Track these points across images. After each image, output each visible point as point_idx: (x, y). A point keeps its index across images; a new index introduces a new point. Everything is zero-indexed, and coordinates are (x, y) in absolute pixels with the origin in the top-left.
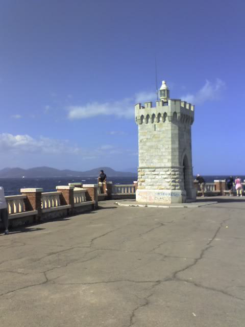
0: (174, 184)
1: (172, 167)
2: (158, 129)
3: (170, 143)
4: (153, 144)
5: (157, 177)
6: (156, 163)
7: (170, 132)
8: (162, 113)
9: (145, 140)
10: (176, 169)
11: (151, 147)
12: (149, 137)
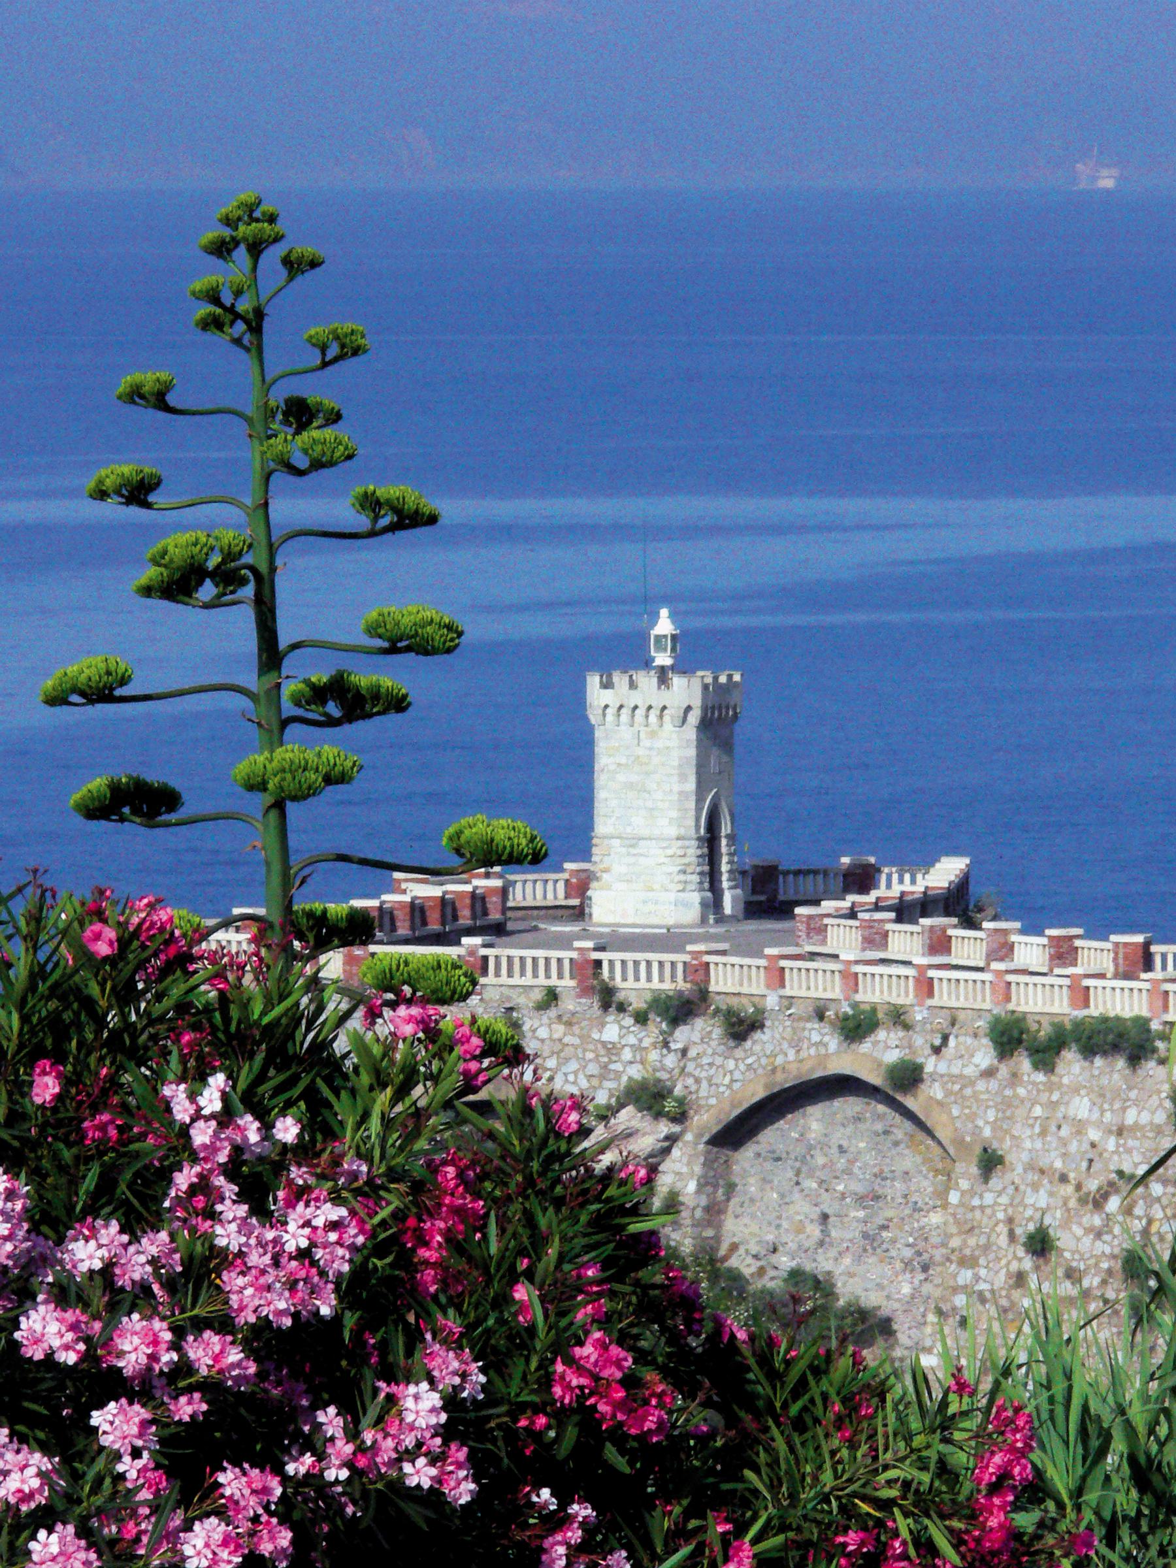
0: (682, 877)
1: (678, 839)
2: (646, 743)
3: (675, 779)
4: (634, 778)
5: (642, 860)
6: (639, 823)
7: (675, 754)
8: (657, 704)
9: (612, 767)
10: (687, 843)
11: (630, 786)
12: (623, 761)
